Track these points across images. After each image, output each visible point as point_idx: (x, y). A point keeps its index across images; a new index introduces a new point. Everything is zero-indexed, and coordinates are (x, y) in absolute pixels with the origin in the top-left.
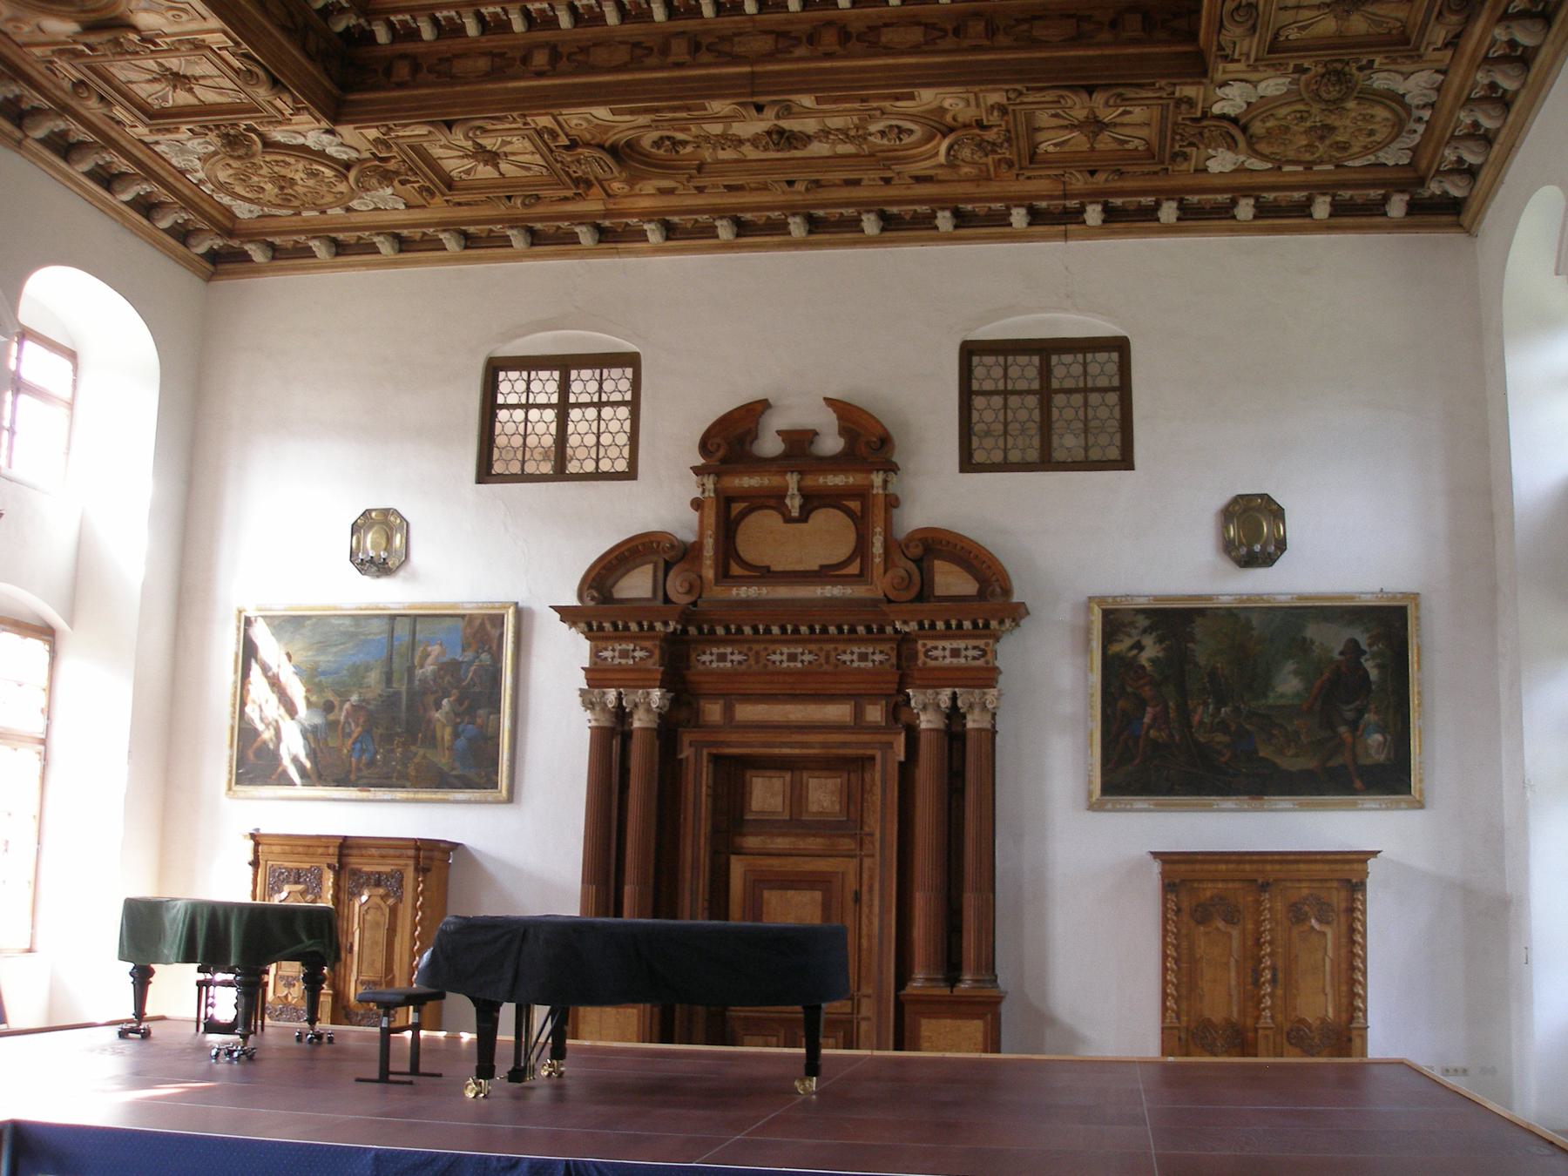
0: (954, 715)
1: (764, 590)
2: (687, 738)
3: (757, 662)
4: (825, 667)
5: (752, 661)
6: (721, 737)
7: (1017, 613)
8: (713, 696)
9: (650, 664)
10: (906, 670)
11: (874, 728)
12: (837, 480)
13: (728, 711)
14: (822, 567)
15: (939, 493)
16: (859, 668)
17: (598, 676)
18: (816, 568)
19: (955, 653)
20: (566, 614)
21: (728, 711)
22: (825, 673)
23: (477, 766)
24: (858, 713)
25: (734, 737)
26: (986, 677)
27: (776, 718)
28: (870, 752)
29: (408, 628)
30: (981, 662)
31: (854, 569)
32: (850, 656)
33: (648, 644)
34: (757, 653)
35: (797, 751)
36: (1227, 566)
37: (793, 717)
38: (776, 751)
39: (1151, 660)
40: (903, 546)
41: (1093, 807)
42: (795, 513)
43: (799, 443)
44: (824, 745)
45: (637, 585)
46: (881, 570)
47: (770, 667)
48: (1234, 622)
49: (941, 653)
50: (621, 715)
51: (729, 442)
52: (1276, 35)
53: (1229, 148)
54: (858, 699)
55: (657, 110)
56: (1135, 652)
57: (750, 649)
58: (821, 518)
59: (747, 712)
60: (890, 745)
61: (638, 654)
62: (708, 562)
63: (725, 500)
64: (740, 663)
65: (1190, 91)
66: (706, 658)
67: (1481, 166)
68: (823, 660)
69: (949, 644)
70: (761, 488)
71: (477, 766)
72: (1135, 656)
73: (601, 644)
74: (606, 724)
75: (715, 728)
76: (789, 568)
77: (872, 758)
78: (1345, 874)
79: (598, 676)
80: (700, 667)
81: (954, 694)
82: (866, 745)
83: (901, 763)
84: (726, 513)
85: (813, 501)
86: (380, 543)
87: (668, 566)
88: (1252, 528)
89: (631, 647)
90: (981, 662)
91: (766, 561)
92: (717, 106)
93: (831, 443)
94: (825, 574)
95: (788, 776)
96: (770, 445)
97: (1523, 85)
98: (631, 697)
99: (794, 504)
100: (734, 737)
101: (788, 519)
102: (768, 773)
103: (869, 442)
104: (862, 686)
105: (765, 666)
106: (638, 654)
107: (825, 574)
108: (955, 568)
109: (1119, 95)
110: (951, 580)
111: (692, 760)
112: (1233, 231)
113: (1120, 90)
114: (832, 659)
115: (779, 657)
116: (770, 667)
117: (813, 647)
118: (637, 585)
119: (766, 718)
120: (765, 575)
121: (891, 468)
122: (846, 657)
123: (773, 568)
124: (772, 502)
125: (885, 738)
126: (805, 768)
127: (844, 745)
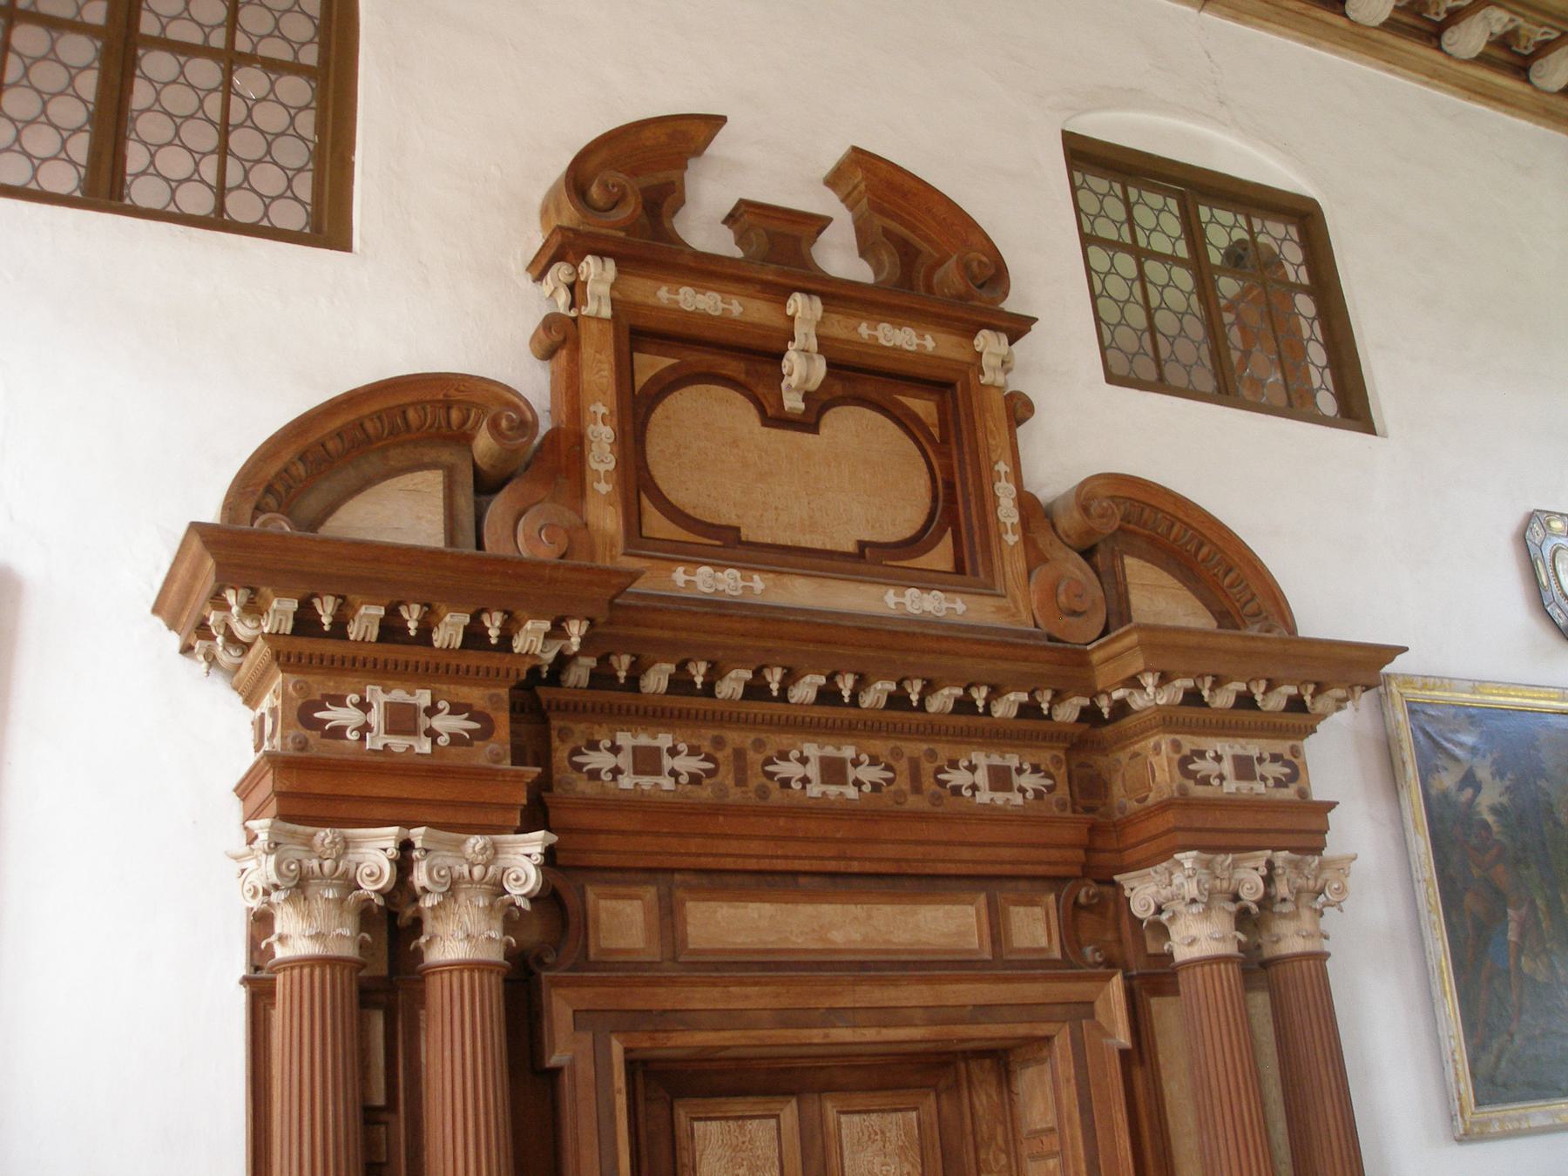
1: (758, 582)
2: (560, 1008)
3: (741, 781)
4: (914, 802)
5: (727, 777)
6: (665, 998)
9: (487, 754)
11: (1031, 966)
13: (668, 919)
14: (862, 545)
16: (990, 807)
17: (319, 784)
18: (850, 547)
19: (1244, 768)
21: (668, 919)
22: (918, 816)
25: (701, 998)
27: (799, 941)
28: (1041, 1030)
30: (1289, 793)
32: (972, 774)
33: (474, 695)
34: (739, 754)
35: (870, 1034)
37: (839, 938)
38: (816, 1035)
39: (1494, 810)
41: (1466, 1137)
42: (793, 403)
44: (935, 1014)
45: (404, 512)
46: (1021, 565)
47: (776, 795)
50: (393, 922)
51: (624, 190)
54: (990, 883)
56: (1469, 792)
57: (719, 743)
58: (852, 427)
59: (725, 924)
60: (1086, 1008)
61: (447, 723)
62: (604, 488)
64: (695, 779)
66: (600, 760)
68: (903, 783)
69: (1228, 747)
70: (725, 321)
72: (1471, 803)
73: (320, 685)
74: (349, 950)
75: (627, 970)
76: (785, 538)
77: (1048, 1039)
79: (319, 784)
80: (584, 787)
81: (1270, 865)
82: (1026, 1010)
83: (1124, 1054)
84: (658, 358)
87: (486, 485)
89: (423, 698)
90: (1289, 793)
91: (728, 516)
94: (868, 560)
95: (789, 1112)
98: (445, 859)
99: (802, 369)
100: (701, 998)
101: (776, 419)
102: (738, 1106)
104: (1006, 853)
105: (763, 792)
106: (447, 723)
107: (868, 560)
108: (1166, 579)
111: (586, 1068)
112: (1435, 76)
114: (928, 783)
115: (801, 766)
116: (776, 795)
117: (881, 746)
118: (404, 512)
119: (771, 940)
120: (726, 543)
122: (958, 777)
123: (747, 534)
124: (734, 367)
125: (1076, 990)
126: (829, 1088)
127: (984, 1011)
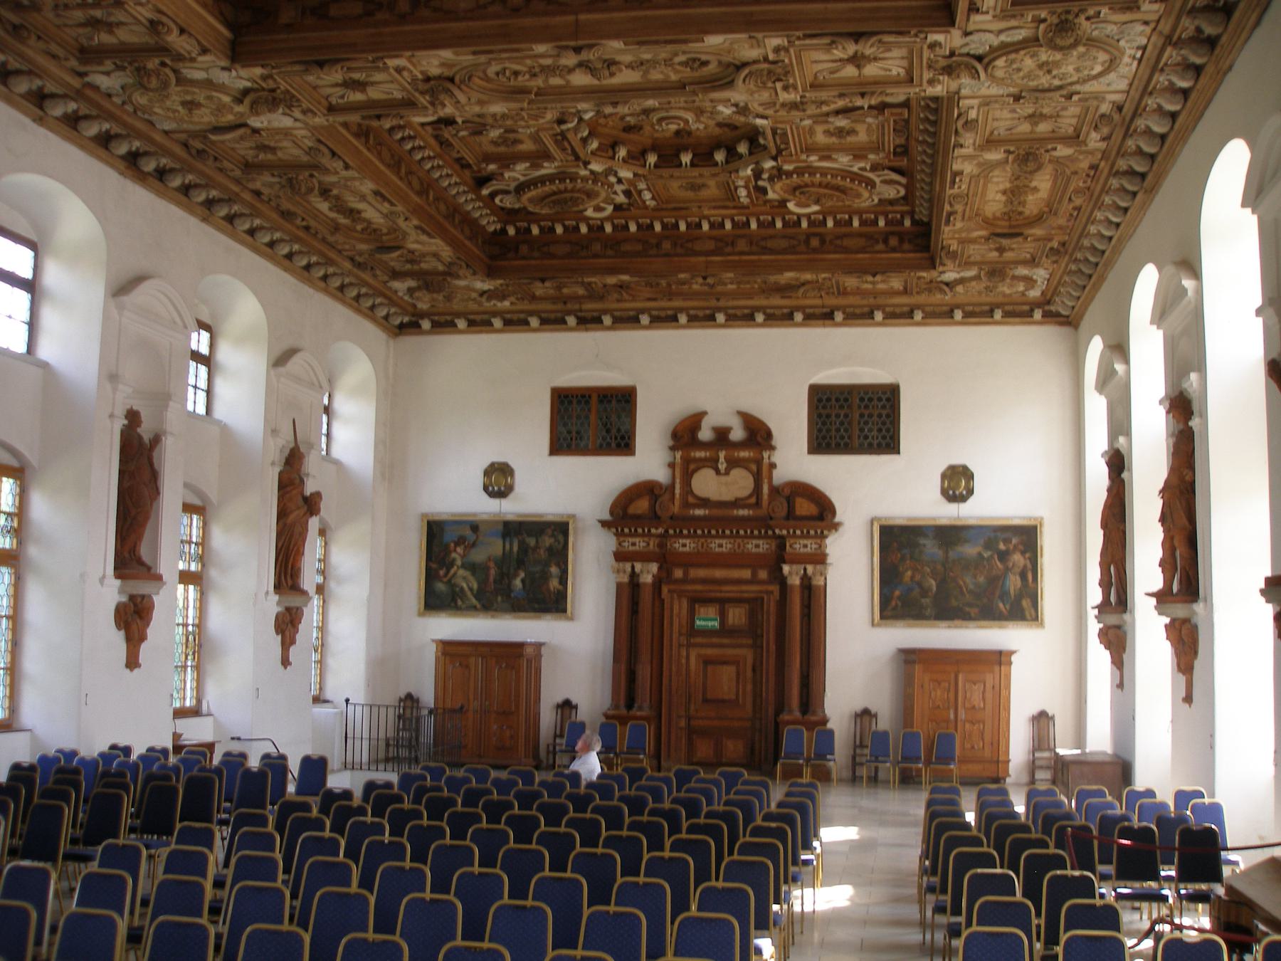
0: (806, 579)
7: (835, 526)
8: (679, 565)
10: (780, 556)
12: (744, 454)
15: (794, 460)
20: (604, 524)
23: (552, 602)
24: (754, 574)
26: (820, 559)
29: (513, 529)
31: (692, 467)
32: (751, 546)
36: (943, 500)
40: (775, 491)
42: (723, 471)
43: (722, 434)
48: (949, 534)
49: (802, 546)
52: (992, 133)
53: (973, 78)
55: (490, 52)
63: (687, 461)
65: (940, 37)
67: (1218, 37)
71: (552, 602)
78: (1001, 659)
84: (687, 470)
85: (733, 463)
86: (499, 479)
88: (957, 482)
92: (541, 48)
93: (737, 434)
96: (705, 434)
97: (1172, 128)
99: (722, 466)
103: (758, 435)
109: (880, 41)
110: (804, 507)
113: (879, 37)
121: (772, 448)
